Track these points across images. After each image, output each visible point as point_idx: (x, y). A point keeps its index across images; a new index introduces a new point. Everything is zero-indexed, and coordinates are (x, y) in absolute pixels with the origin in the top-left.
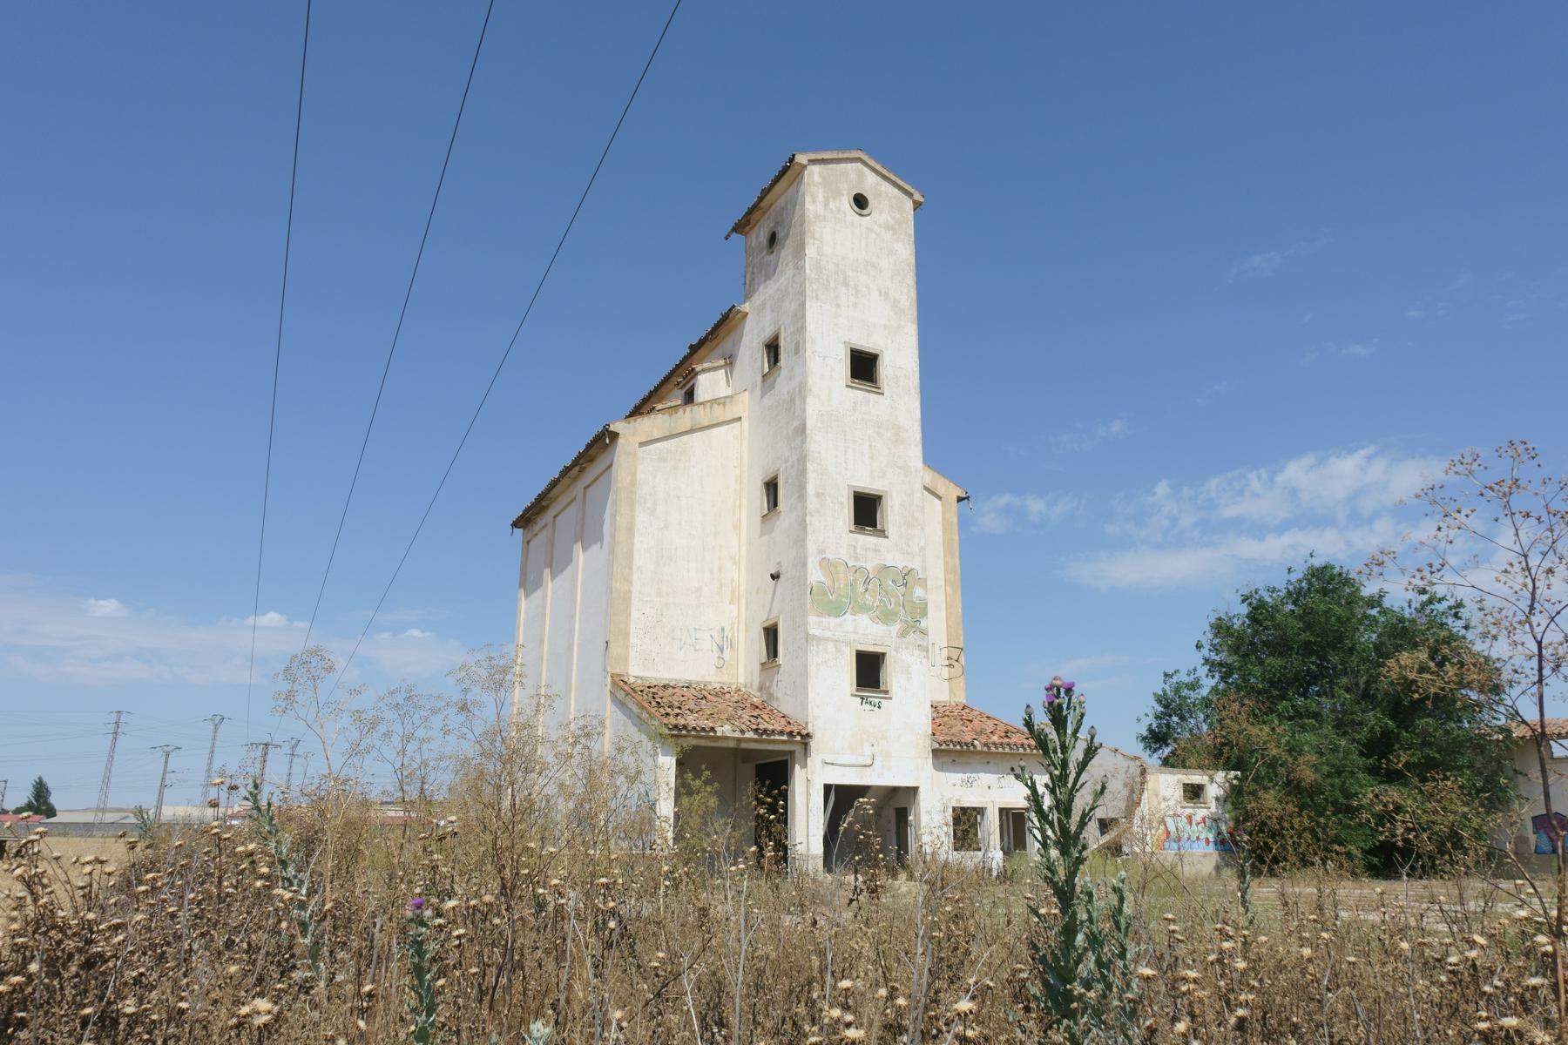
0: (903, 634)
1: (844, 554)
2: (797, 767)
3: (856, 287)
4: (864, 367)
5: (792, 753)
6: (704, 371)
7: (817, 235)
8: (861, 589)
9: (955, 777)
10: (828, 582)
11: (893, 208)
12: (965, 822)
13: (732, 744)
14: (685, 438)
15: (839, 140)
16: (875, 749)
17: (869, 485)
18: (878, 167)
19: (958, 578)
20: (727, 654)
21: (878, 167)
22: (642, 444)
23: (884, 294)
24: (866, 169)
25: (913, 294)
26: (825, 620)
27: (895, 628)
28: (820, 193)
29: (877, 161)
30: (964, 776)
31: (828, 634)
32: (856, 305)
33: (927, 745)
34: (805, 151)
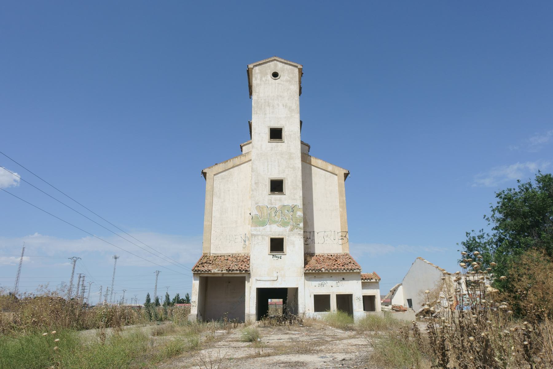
0: (291, 230)
1: (266, 204)
2: (246, 282)
3: (273, 106)
4: (276, 134)
5: (245, 277)
6: (244, 145)
7: (257, 91)
8: (273, 215)
9: (316, 283)
10: (259, 214)
11: (290, 74)
12: (321, 302)
13: (220, 275)
14: (231, 170)
15: (263, 56)
16: (278, 274)
17: (276, 176)
18: (283, 60)
19: (345, 205)
20: (247, 243)
21: (283, 60)
22: (215, 175)
23: (285, 106)
24: (278, 63)
25: (298, 103)
26: (258, 228)
27: (289, 228)
28: (259, 76)
29: (282, 58)
30: (320, 283)
31: (259, 233)
32: (273, 112)
33: (302, 271)
34: (250, 64)
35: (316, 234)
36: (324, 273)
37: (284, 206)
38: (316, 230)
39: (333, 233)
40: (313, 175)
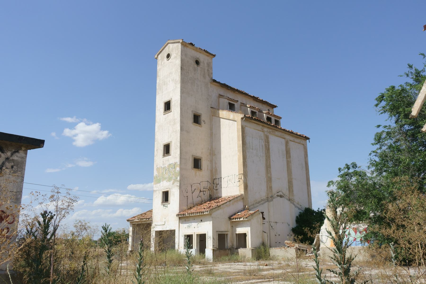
21: (172, 41)
27: (172, 181)
30: (188, 225)
35: (222, 179)
36: (187, 217)
37: (170, 164)
38: (223, 177)
39: (234, 176)
40: (221, 126)
